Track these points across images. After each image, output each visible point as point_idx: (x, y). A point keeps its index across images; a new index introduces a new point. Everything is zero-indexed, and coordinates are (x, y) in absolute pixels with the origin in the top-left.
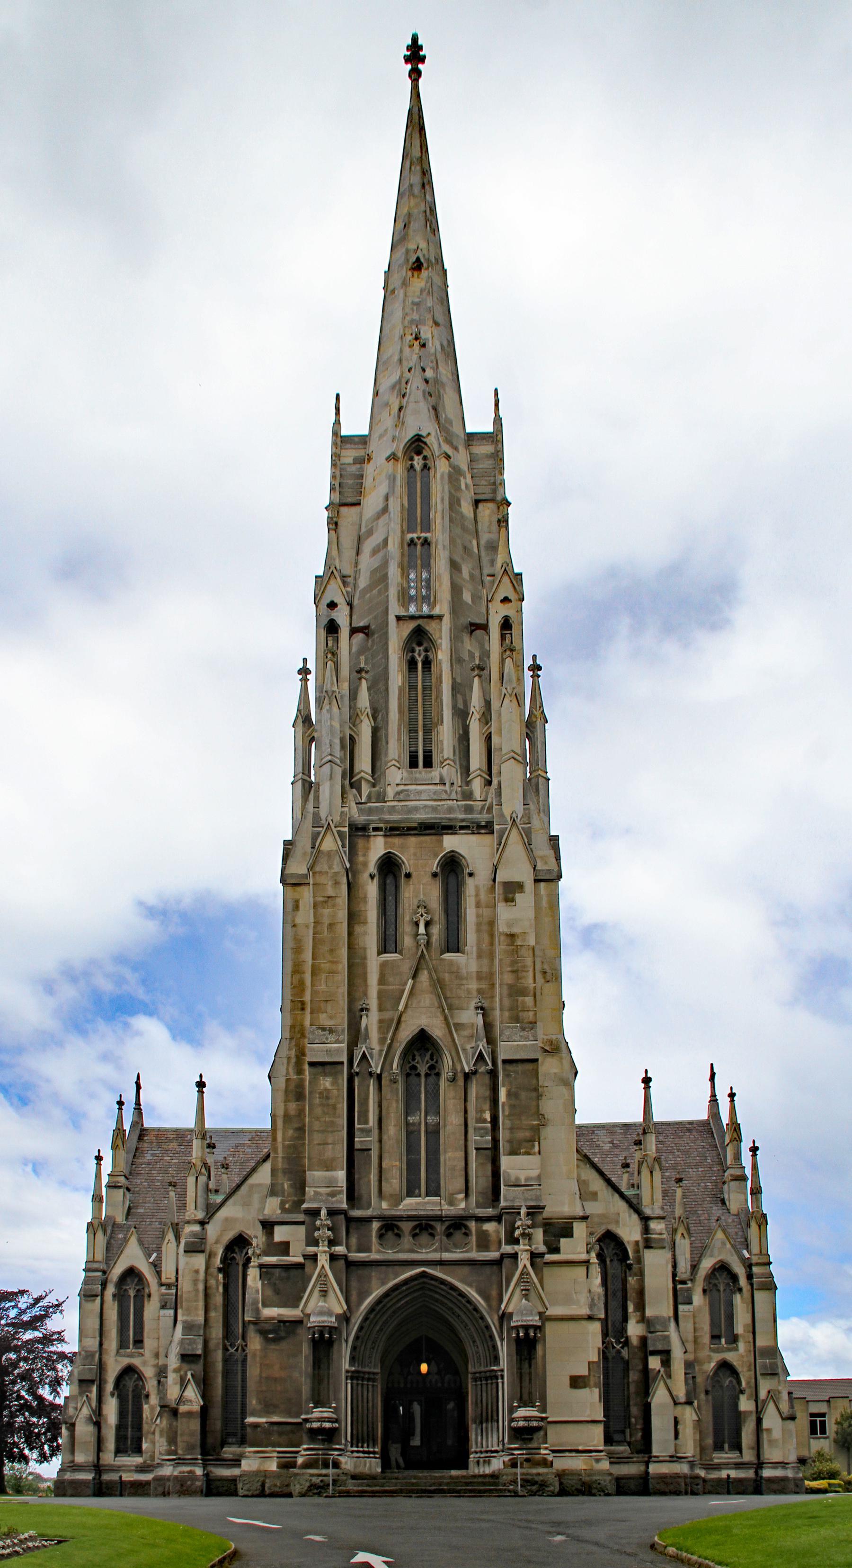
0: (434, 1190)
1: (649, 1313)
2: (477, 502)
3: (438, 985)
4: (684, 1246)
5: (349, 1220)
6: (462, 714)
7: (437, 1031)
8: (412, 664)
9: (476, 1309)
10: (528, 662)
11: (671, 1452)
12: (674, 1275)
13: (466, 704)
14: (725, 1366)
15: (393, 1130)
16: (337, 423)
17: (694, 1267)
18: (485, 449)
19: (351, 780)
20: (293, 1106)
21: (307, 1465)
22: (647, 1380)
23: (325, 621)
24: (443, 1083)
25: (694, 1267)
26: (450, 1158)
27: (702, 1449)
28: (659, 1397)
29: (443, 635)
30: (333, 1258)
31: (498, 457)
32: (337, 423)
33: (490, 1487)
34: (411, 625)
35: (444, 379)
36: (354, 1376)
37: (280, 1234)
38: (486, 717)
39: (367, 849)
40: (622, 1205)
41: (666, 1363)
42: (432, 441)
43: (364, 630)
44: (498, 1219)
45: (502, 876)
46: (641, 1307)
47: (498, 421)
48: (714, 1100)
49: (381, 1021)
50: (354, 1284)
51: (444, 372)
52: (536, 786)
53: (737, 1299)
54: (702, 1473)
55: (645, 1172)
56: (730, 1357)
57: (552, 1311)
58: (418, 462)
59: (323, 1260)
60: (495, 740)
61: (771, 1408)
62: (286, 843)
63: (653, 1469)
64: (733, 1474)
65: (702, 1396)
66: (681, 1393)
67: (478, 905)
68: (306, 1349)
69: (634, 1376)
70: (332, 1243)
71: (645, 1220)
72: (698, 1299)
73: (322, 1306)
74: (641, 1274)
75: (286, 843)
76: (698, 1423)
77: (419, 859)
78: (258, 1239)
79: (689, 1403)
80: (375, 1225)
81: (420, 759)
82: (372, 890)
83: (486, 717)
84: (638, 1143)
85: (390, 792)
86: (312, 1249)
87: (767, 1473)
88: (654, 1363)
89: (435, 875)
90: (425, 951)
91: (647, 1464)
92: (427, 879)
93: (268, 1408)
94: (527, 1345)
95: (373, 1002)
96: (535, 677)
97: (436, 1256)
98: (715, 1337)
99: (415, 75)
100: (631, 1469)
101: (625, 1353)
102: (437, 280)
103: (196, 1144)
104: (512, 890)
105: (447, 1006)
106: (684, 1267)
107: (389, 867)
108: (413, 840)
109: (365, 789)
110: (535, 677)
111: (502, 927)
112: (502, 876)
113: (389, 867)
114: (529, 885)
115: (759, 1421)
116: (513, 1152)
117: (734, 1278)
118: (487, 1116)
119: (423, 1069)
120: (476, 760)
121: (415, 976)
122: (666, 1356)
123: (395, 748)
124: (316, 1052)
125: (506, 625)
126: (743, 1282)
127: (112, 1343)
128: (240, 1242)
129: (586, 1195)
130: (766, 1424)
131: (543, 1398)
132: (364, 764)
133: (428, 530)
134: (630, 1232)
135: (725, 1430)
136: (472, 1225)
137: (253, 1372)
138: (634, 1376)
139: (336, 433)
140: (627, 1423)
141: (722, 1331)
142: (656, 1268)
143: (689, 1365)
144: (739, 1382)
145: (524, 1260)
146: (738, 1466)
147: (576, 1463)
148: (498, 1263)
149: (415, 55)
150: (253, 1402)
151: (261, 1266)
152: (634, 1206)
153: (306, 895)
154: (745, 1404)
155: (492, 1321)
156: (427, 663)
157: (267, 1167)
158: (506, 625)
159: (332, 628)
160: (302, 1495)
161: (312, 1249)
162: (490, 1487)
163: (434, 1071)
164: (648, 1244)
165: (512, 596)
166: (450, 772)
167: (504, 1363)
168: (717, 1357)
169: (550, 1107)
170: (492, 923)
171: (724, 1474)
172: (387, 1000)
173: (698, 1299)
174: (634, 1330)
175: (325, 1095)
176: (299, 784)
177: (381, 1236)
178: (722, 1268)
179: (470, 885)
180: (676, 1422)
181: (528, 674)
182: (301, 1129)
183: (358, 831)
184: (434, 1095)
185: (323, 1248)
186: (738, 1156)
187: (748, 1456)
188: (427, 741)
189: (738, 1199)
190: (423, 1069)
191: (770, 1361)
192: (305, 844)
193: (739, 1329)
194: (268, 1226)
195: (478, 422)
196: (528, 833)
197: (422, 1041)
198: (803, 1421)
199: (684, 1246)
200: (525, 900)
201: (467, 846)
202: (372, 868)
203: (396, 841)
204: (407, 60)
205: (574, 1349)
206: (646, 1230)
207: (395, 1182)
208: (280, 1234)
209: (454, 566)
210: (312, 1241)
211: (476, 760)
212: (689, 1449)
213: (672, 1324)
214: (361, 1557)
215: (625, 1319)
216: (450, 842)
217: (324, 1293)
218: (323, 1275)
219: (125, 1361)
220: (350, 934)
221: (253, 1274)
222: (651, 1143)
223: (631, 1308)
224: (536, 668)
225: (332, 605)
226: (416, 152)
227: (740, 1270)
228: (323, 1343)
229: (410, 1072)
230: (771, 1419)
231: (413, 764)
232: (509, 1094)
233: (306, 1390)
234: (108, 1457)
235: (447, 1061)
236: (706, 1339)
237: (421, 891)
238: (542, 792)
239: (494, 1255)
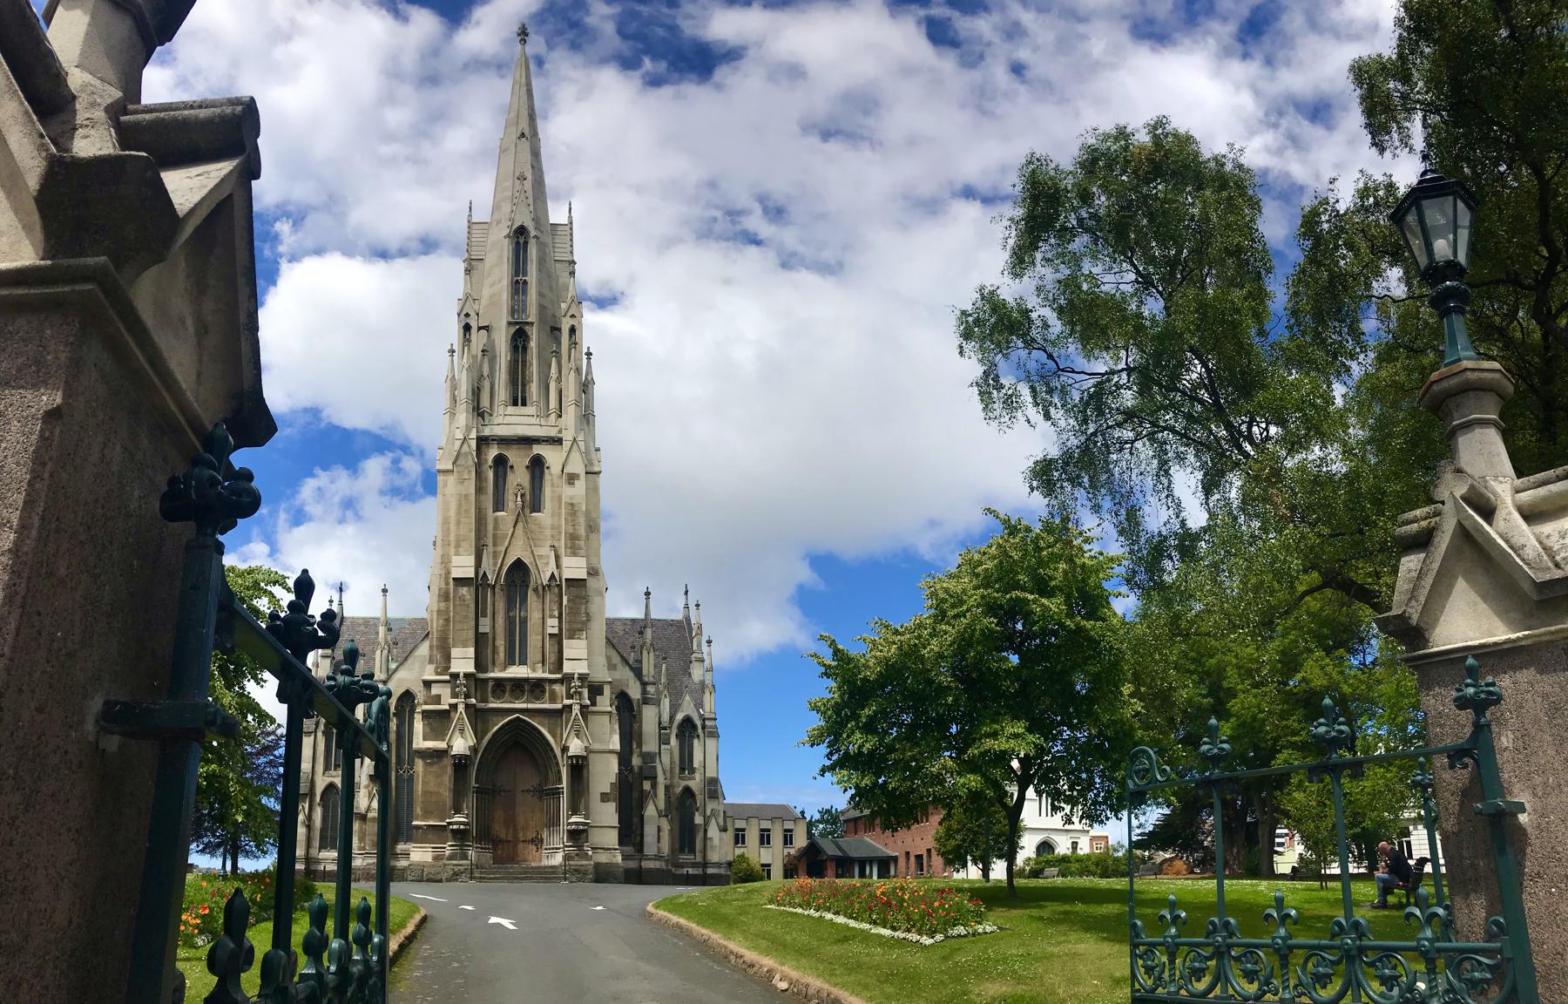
0: (523, 662)
1: (645, 749)
4: (666, 703)
5: (477, 680)
14: (688, 791)
15: (500, 621)
17: (672, 718)
20: (443, 605)
21: (451, 858)
24: (530, 592)
25: (672, 718)
27: (672, 850)
28: (650, 811)
29: (534, 333)
30: (467, 706)
33: (547, 875)
37: (435, 690)
38: (559, 379)
40: (631, 674)
41: (654, 786)
43: (486, 328)
44: (561, 681)
46: (640, 745)
53: (696, 742)
55: (645, 653)
56: (691, 784)
57: (596, 746)
59: (461, 708)
61: (713, 823)
64: (691, 871)
66: (662, 805)
68: (450, 770)
69: (635, 795)
70: (467, 696)
71: (644, 684)
77: (519, 460)
78: (420, 695)
80: (491, 684)
82: (491, 474)
83: (559, 379)
84: (641, 633)
86: (454, 701)
87: (710, 871)
88: (647, 786)
93: (427, 814)
94: (579, 768)
97: (524, 706)
98: (682, 769)
100: (632, 864)
103: (382, 630)
104: (572, 478)
106: (666, 717)
107: (501, 461)
112: (568, 470)
113: (501, 461)
114: (583, 475)
116: (571, 637)
117: (694, 727)
122: (654, 779)
124: (456, 573)
125: (573, 330)
127: (320, 767)
128: (407, 696)
129: (611, 667)
131: (587, 808)
133: (525, 274)
134: (635, 692)
135: (687, 836)
137: (419, 788)
140: (630, 831)
142: (649, 716)
143: (667, 788)
145: (576, 709)
147: (603, 858)
148: (558, 713)
150: (418, 810)
151: (424, 712)
152: (638, 673)
154: (698, 820)
155: (558, 752)
157: (426, 644)
158: (573, 330)
159: (467, 328)
160: (448, 880)
162: (547, 875)
163: (525, 584)
164: (646, 701)
167: (564, 784)
169: (593, 608)
170: (560, 497)
173: (674, 741)
174: (636, 761)
175: (462, 599)
177: (493, 692)
178: (688, 721)
182: (447, 620)
184: (524, 600)
186: (699, 645)
188: (524, 391)
190: (518, 582)
193: (696, 765)
194: (428, 684)
197: (519, 565)
198: (730, 834)
199: (666, 703)
200: (580, 485)
205: (605, 773)
206: (644, 692)
208: (435, 690)
210: (455, 695)
212: (666, 850)
214: (493, 920)
216: (537, 449)
219: (329, 780)
221: (418, 718)
222: (649, 633)
224: (589, 354)
227: (698, 723)
228: (461, 764)
230: (713, 832)
233: (449, 801)
234: (314, 852)
237: (519, 477)
239: (559, 706)
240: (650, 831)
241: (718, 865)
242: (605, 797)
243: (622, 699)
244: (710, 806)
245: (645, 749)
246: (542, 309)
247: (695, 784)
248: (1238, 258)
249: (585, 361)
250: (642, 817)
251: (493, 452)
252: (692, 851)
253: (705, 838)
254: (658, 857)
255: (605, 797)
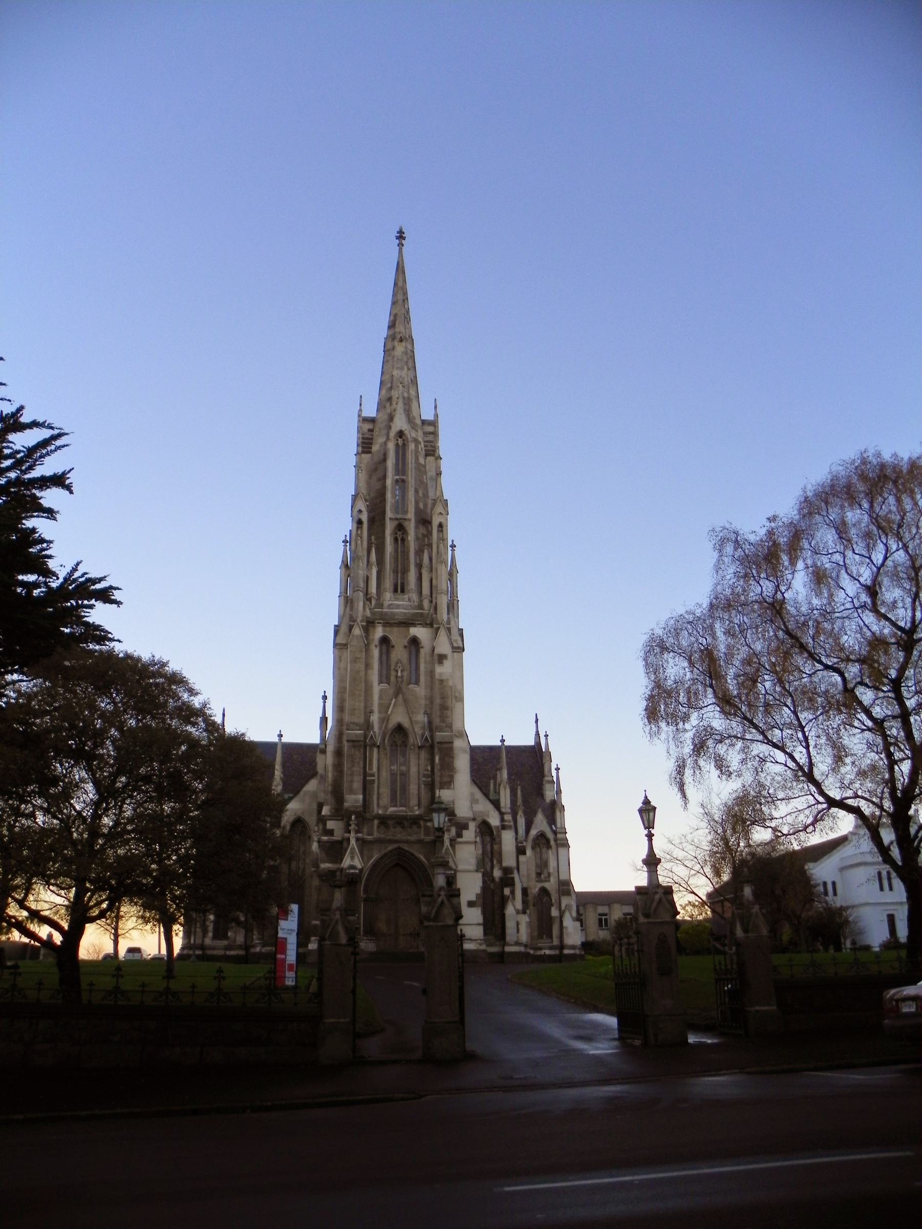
1: (504, 864)
2: (426, 455)
3: (406, 702)
6: (419, 566)
7: (406, 723)
8: (396, 539)
9: (423, 866)
10: (450, 543)
11: (515, 939)
12: (516, 839)
13: (421, 560)
14: (544, 891)
16: (361, 410)
18: (431, 429)
19: (368, 598)
22: (504, 901)
23: (356, 519)
26: (413, 788)
27: (532, 938)
28: (510, 910)
30: (357, 839)
31: (435, 434)
32: (361, 410)
34: (396, 523)
35: (412, 397)
36: (366, 900)
39: (374, 632)
41: (513, 892)
42: (406, 432)
45: (437, 651)
46: (500, 861)
47: (436, 416)
48: (537, 734)
49: (379, 718)
50: (366, 852)
51: (413, 392)
52: (453, 606)
54: (532, 952)
56: (546, 885)
58: (400, 441)
59: (353, 842)
60: (434, 582)
62: (335, 626)
63: (508, 949)
65: (532, 907)
66: (519, 906)
67: (425, 662)
71: (502, 814)
72: (529, 852)
73: (352, 861)
74: (500, 843)
75: (335, 626)
76: (529, 924)
77: (398, 639)
79: (524, 912)
81: (400, 588)
82: (376, 653)
83: (431, 570)
85: (386, 603)
87: (566, 952)
88: (507, 891)
89: (405, 647)
90: (445, 900)
91: (503, 946)
92: (401, 648)
95: (376, 708)
96: (453, 550)
99: (401, 245)
101: (492, 886)
102: (409, 347)
105: (410, 712)
108: (396, 629)
109: (373, 602)
110: (453, 550)
111: (437, 676)
115: (561, 922)
117: (548, 841)
118: (429, 768)
119: (399, 743)
120: (426, 590)
121: (396, 697)
123: (388, 584)
126: (552, 843)
130: (565, 924)
132: (373, 589)
133: (404, 474)
136: (422, 823)
138: (497, 899)
139: (359, 416)
141: (542, 870)
142: (508, 840)
144: (551, 900)
146: (551, 948)
149: (401, 236)
152: (496, 804)
153: (347, 654)
154: (554, 912)
156: (403, 540)
161: (346, 835)
163: (405, 744)
164: (504, 827)
165: (443, 512)
166: (415, 597)
168: (540, 885)
171: (542, 952)
172: (384, 708)
176: (342, 598)
177: (378, 827)
178: (542, 835)
179: (422, 651)
180: (518, 924)
181: (450, 549)
183: (369, 624)
185: (352, 835)
187: (556, 942)
188: (403, 578)
189: (549, 795)
191: (566, 887)
192: (344, 628)
195: (427, 414)
196: (449, 630)
201: (419, 632)
202: (376, 642)
203: (388, 629)
204: (397, 238)
206: (502, 820)
207: (385, 800)
209: (416, 491)
211: (426, 590)
213: (516, 871)
215: (492, 867)
217: (352, 858)
218: (353, 849)
220: (366, 674)
223: (495, 862)
224: (453, 546)
225: (360, 511)
226: (400, 297)
227: (550, 836)
229: (394, 744)
231: (395, 590)
232: (440, 759)
235: (411, 740)
236: (533, 875)
237: (399, 653)
238: (456, 607)
240: (510, 925)
241: (573, 947)
242: (471, 904)
243: (485, 828)
244: (565, 901)
245: (504, 864)
246: (418, 512)
247: (551, 885)
248: (871, 666)
249: (450, 553)
250: (503, 916)
251: (379, 632)
252: (550, 936)
253: (561, 927)
254: (517, 943)
255: (471, 904)
